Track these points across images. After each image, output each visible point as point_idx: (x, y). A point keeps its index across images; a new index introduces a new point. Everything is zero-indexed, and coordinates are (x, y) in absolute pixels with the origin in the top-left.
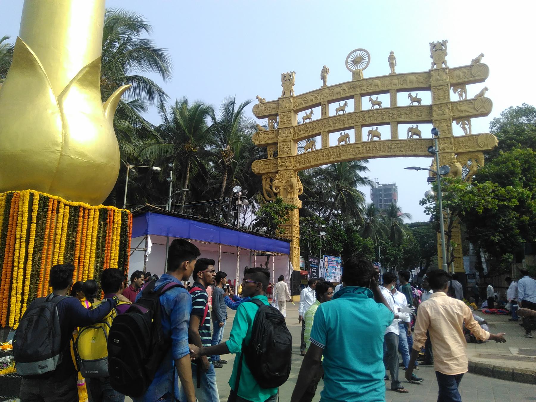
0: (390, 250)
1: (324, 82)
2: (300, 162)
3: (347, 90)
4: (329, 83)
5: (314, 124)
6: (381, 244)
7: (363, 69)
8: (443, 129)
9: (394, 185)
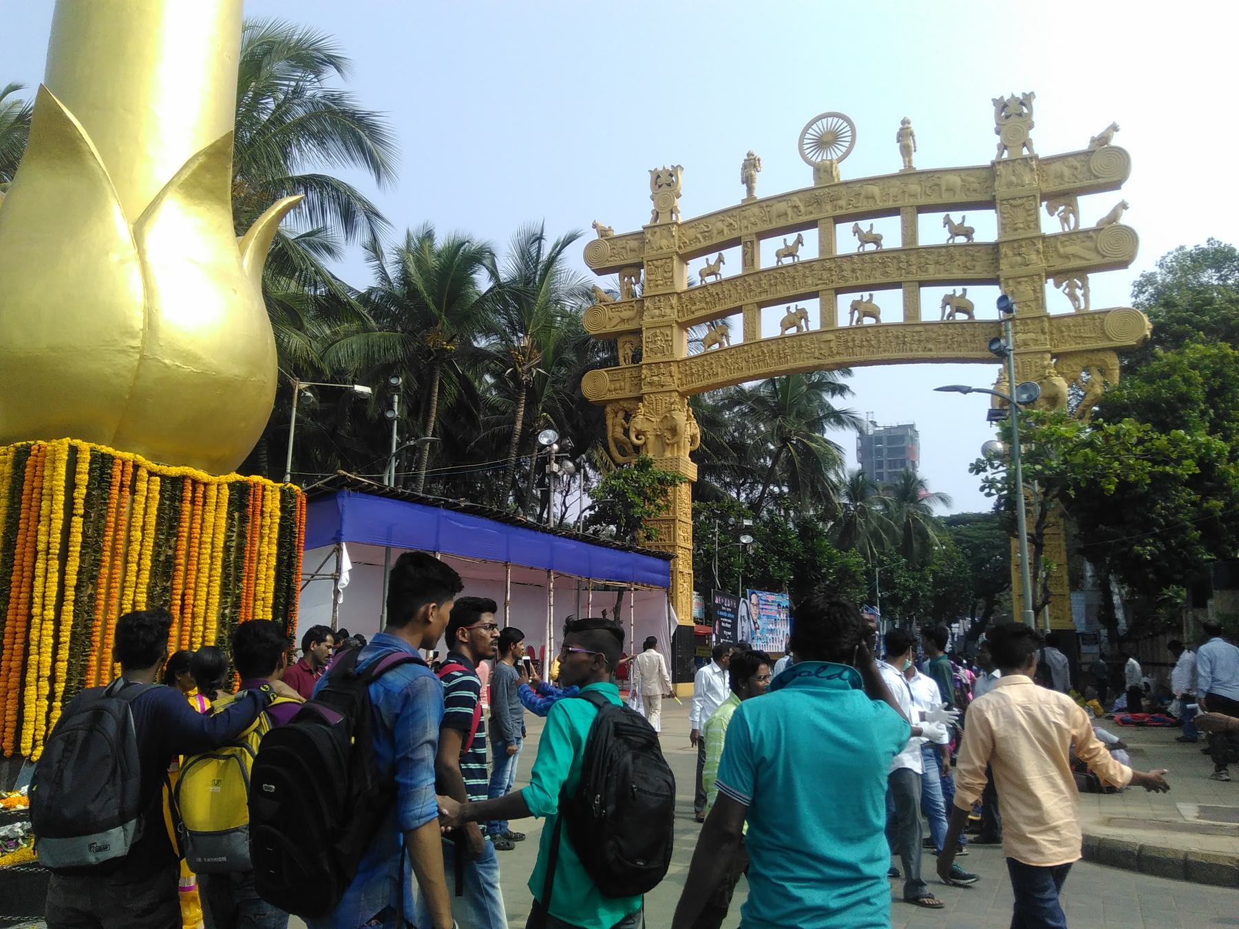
0: (901, 578)
1: (750, 190)
2: (692, 374)
3: (802, 208)
4: (761, 193)
5: (726, 286)
6: (881, 563)
7: (840, 160)
8: (1023, 299)
9: (912, 427)
